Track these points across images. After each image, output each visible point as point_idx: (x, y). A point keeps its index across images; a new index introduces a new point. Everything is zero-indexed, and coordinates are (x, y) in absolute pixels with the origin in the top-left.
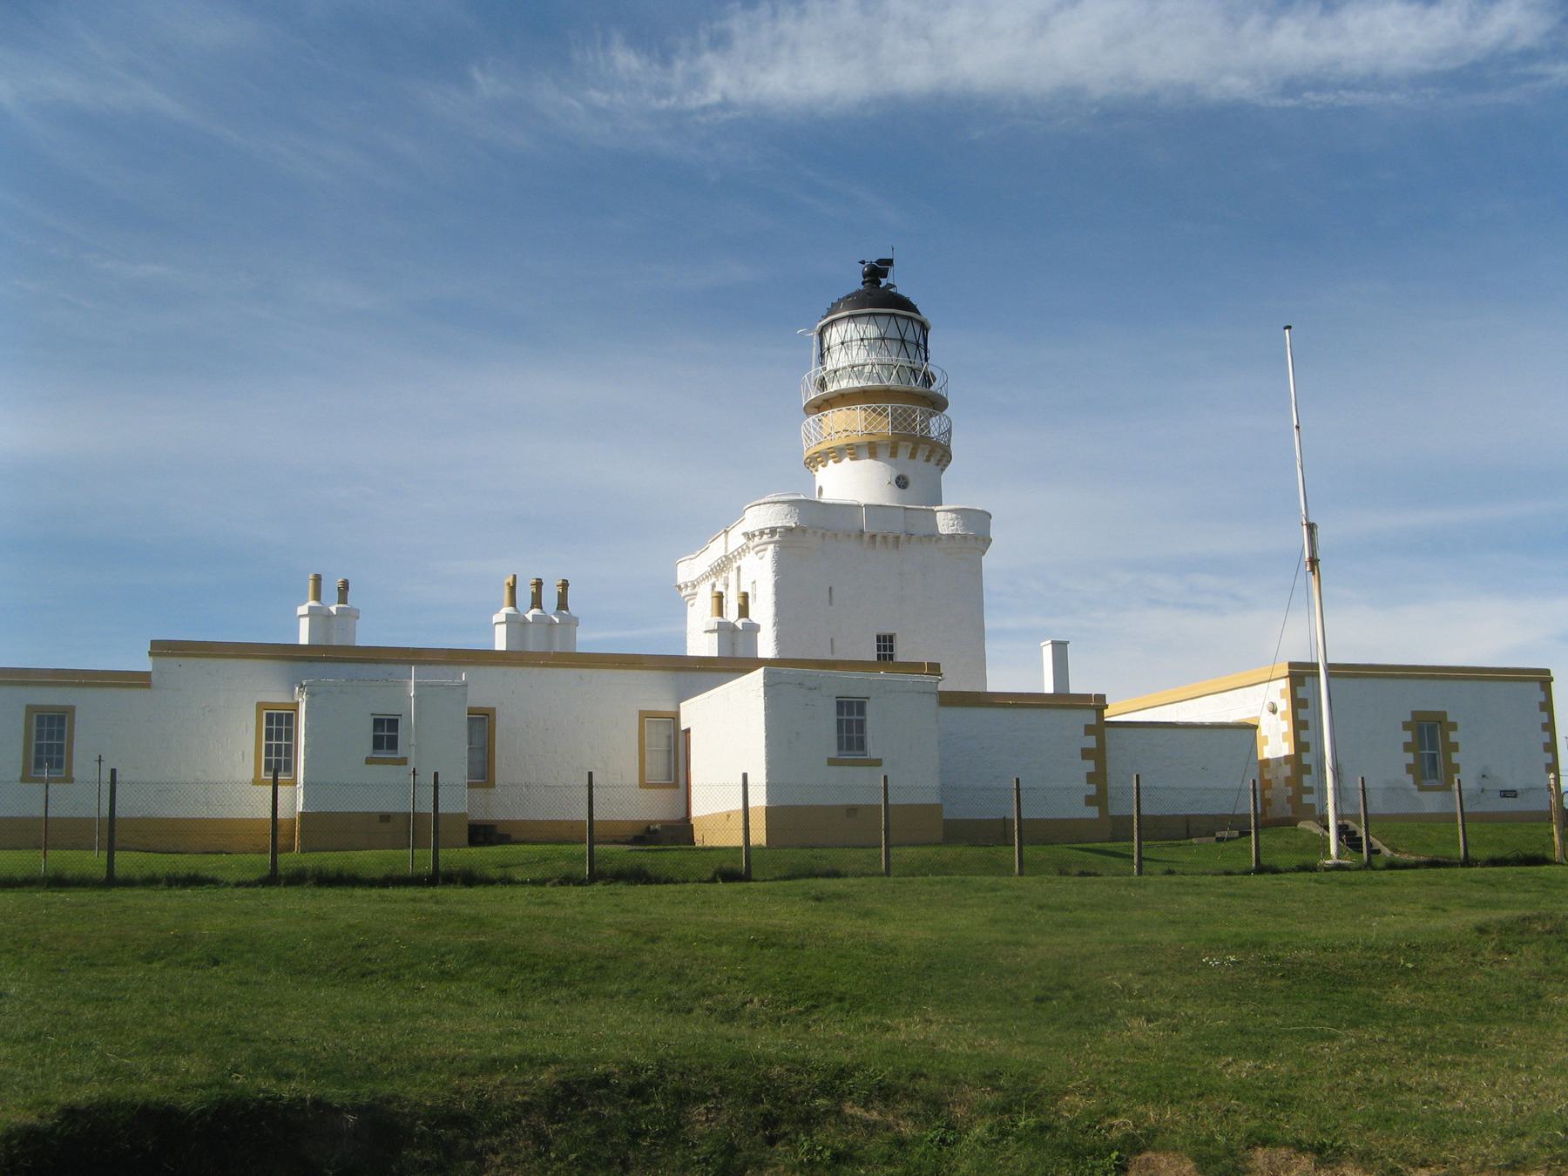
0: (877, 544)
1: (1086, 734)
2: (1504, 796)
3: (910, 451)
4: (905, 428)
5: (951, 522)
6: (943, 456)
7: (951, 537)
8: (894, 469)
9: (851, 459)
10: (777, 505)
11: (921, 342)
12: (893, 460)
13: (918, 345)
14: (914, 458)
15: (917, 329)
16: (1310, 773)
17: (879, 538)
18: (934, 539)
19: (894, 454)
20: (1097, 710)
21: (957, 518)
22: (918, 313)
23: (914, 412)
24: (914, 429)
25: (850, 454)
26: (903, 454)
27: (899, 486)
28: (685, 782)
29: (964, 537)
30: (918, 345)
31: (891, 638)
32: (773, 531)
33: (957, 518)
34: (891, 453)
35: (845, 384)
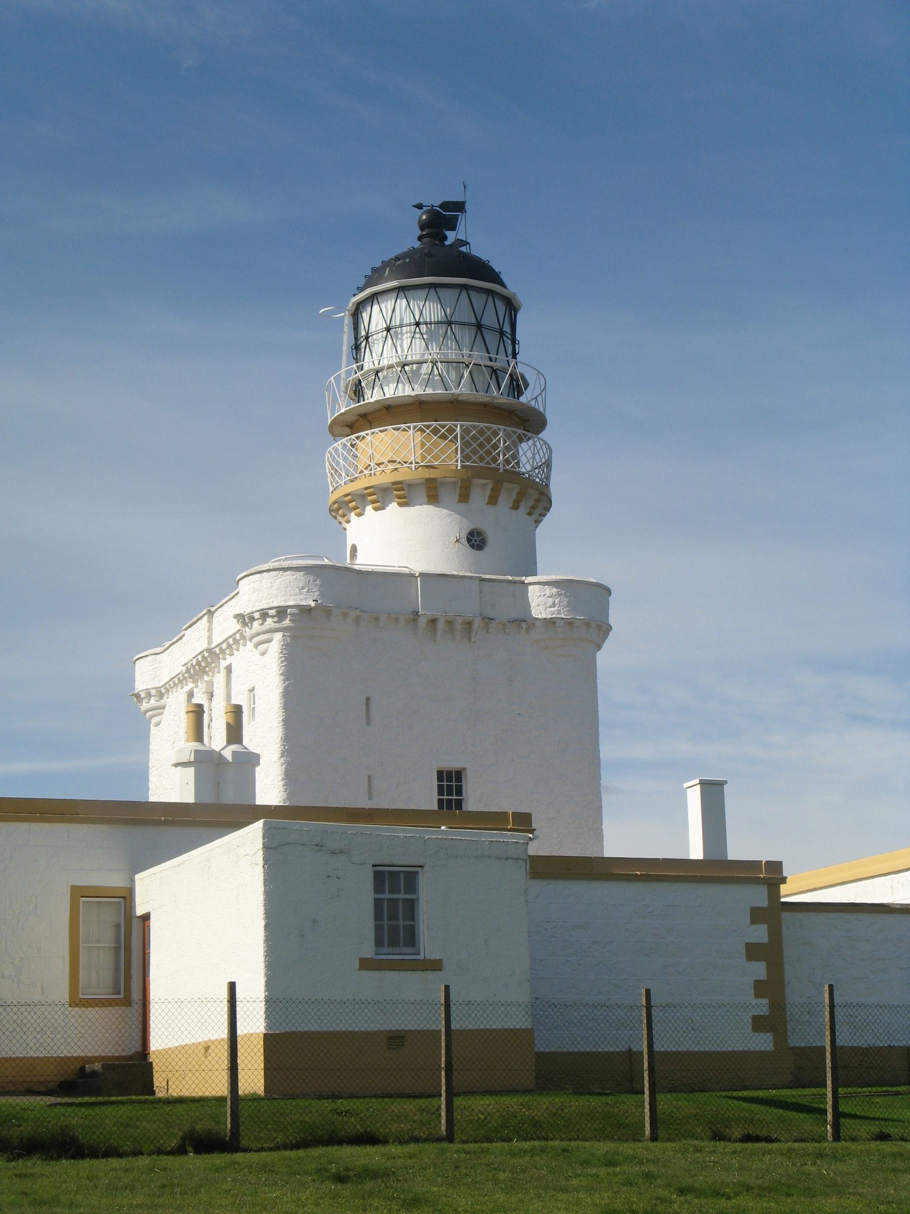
0: (439, 632)
5: (551, 600)
6: (538, 501)
10: (289, 573)
11: (507, 328)
12: (463, 506)
13: (502, 333)
15: (501, 308)
17: (441, 625)
18: (524, 625)
19: (464, 497)
22: (502, 284)
23: (495, 434)
24: (495, 460)
26: (478, 498)
27: (473, 546)
29: (570, 623)
30: (502, 333)
32: (281, 612)
35: (391, 391)
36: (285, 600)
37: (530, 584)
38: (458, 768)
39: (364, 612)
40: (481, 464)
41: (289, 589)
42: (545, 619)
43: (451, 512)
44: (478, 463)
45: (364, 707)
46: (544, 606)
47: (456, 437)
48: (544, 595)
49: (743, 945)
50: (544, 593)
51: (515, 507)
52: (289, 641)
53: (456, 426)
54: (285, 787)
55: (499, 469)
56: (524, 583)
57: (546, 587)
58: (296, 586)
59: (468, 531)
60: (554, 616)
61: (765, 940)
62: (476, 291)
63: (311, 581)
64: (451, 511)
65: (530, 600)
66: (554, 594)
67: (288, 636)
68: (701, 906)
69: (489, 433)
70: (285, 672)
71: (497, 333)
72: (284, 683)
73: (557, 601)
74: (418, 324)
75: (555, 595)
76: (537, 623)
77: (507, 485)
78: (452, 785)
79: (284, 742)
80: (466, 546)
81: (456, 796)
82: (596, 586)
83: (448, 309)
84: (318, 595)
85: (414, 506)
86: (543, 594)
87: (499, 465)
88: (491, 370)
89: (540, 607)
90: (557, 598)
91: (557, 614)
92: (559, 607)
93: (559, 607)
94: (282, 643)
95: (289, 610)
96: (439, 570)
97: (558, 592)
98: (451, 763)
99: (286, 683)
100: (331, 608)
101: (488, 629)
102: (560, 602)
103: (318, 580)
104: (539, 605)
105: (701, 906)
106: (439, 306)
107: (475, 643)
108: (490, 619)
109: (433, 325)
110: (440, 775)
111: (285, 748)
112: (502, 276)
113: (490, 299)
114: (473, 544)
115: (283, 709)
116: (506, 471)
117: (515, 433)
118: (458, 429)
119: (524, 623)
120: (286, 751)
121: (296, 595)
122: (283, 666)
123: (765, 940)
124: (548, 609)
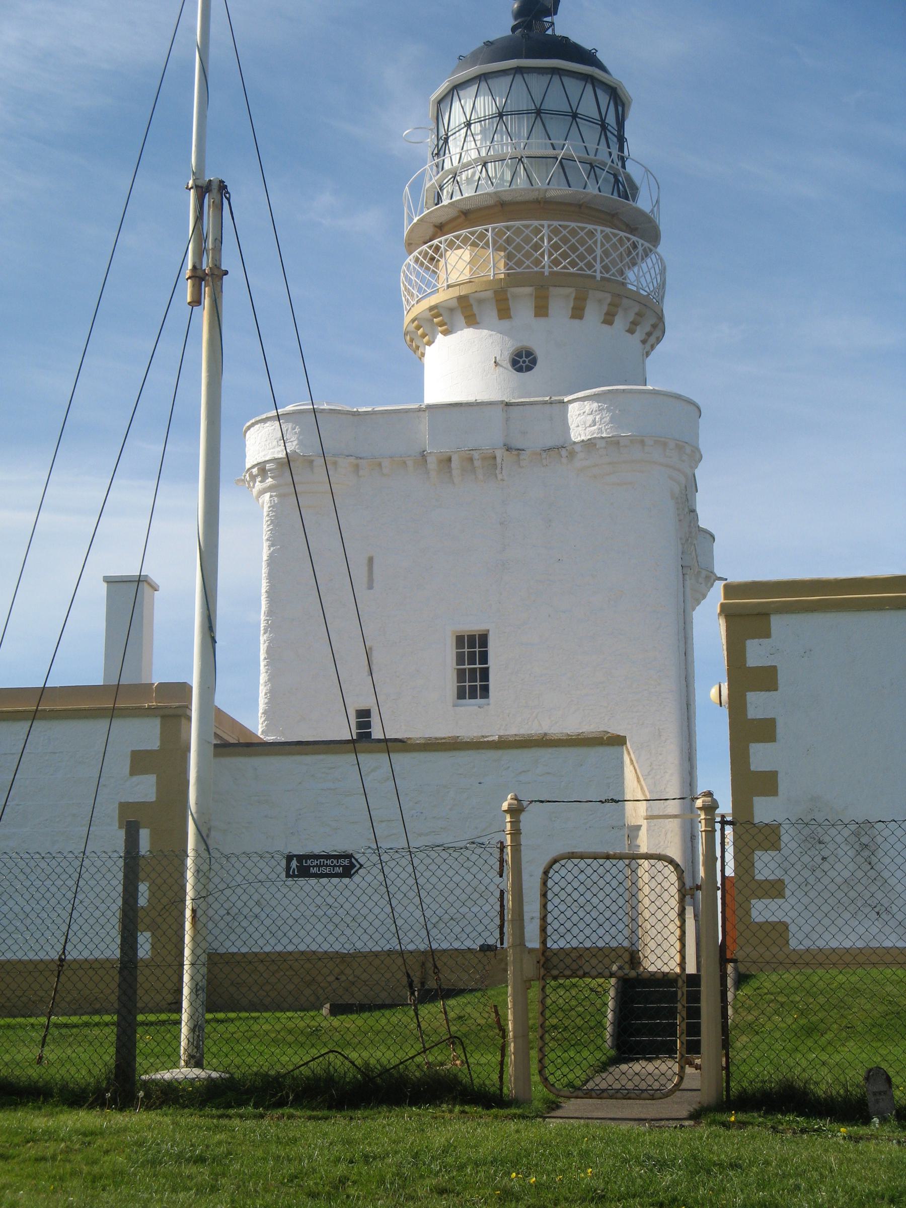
0: (456, 472)
1: (134, 771)
2: (304, 872)
3: (605, 308)
4: (573, 264)
5: (590, 418)
7: (589, 444)
8: (506, 338)
9: (446, 333)
10: (268, 424)
11: (611, 120)
12: (506, 323)
13: (604, 127)
14: (581, 317)
15: (604, 98)
16: (775, 845)
17: (455, 463)
18: (564, 453)
19: (504, 312)
20: (163, 717)
21: (600, 410)
23: (537, 231)
24: (537, 262)
25: (441, 324)
26: (524, 311)
27: (529, 369)
28: (537, 915)
29: (613, 443)
30: (604, 127)
31: (483, 639)
33: (600, 410)
34: (499, 311)
36: (264, 456)
37: (570, 402)
38: (483, 630)
39: (360, 458)
40: (519, 270)
41: (268, 441)
42: (583, 441)
43: (493, 332)
44: (515, 269)
45: (366, 568)
46: (584, 426)
47: (487, 244)
48: (584, 413)
49: (117, 805)
50: (584, 411)
51: (608, 320)
52: (276, 502)
53: (487, 230)
54: (267, 667)
55: (543, 273)
56: (564, 403)
57: (586, 403)
58: (273, 438)
59: (511, 350)
60: (595, 435)
61: (152, 797)
62: (539, 73)
63: (289, 430)
64: (492, 331)
65: (570, 421)
66: (594, 410)
67: (275, 496)
68: (55, 753)
69: (590, 242)
70: (270, 537)
71: (570, 117)
72: (269, 549)
73: (598, 417)
74: (468, 125)
75: (596, 411)
76: (577, 448)
77: (553, 291)
78: (468, 648)
79: (267, 617)
80: (511, 371)
81: (479, 664)
82: (655, 393)
83: (497, 98)
84: (296, 445)
85: (456, 332)
86: (582, 411)
87: (543, 267)
88: (588, 167)
89: (580, 428)
90: (599, 414)
91: (598, 433)
92: (600, 424)
93: (600, 424)
94: (269, 504)
95: (267, 465)
96: (471, 399)
97: (599, 406)
98: (473, 626)
99: (272, 549)
100: (312, 458)
101: (519, 464)
102: (601, 419)
103: (297, 427)
104: (578, 426)
105: (55, 753)
106: (490, 97)
107: (503, 480)
108: (518, 449)
109: (487, 121)
110: (460, 640)
111: (268, 622)
112: (599, 56)
113: (589, 88)
114: (527, 366)
115: (267, 579)
116: (603, 279)
117: (615, 235)
118: (489, 234)
119: (564, 449)
120: (268, 627)
121: (274, 448)
122: (268, 531)
123: (152, 797)
124: (588, 429)
